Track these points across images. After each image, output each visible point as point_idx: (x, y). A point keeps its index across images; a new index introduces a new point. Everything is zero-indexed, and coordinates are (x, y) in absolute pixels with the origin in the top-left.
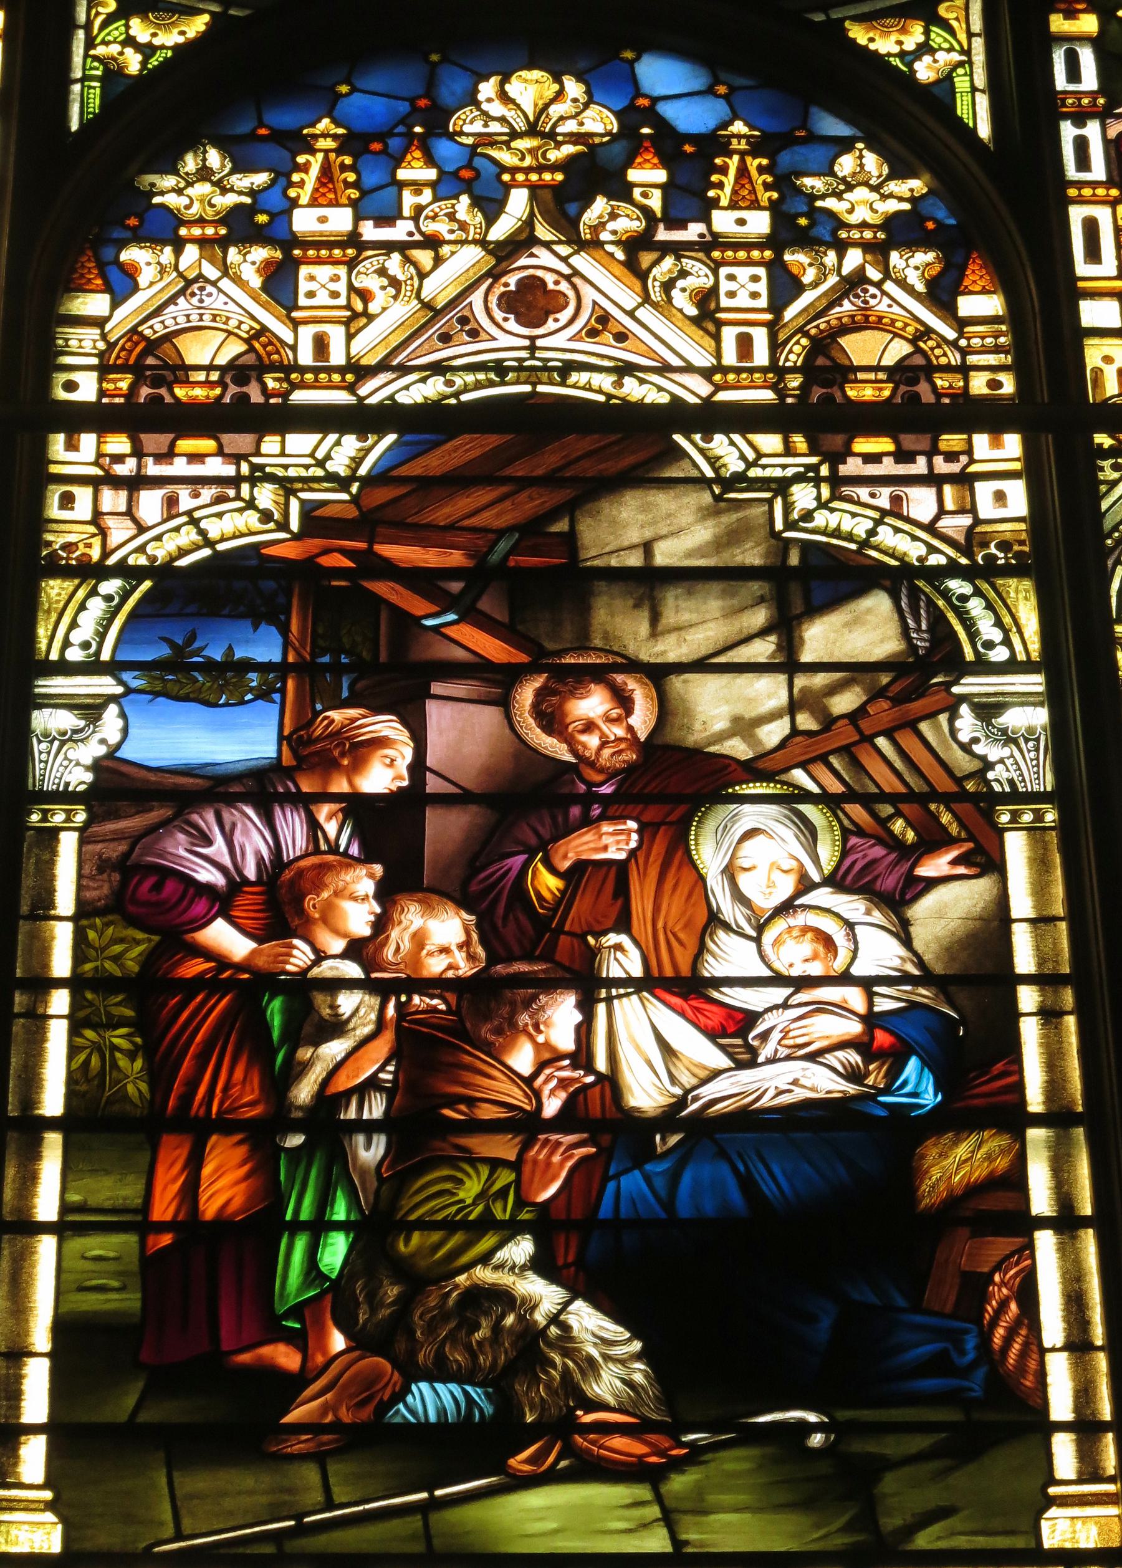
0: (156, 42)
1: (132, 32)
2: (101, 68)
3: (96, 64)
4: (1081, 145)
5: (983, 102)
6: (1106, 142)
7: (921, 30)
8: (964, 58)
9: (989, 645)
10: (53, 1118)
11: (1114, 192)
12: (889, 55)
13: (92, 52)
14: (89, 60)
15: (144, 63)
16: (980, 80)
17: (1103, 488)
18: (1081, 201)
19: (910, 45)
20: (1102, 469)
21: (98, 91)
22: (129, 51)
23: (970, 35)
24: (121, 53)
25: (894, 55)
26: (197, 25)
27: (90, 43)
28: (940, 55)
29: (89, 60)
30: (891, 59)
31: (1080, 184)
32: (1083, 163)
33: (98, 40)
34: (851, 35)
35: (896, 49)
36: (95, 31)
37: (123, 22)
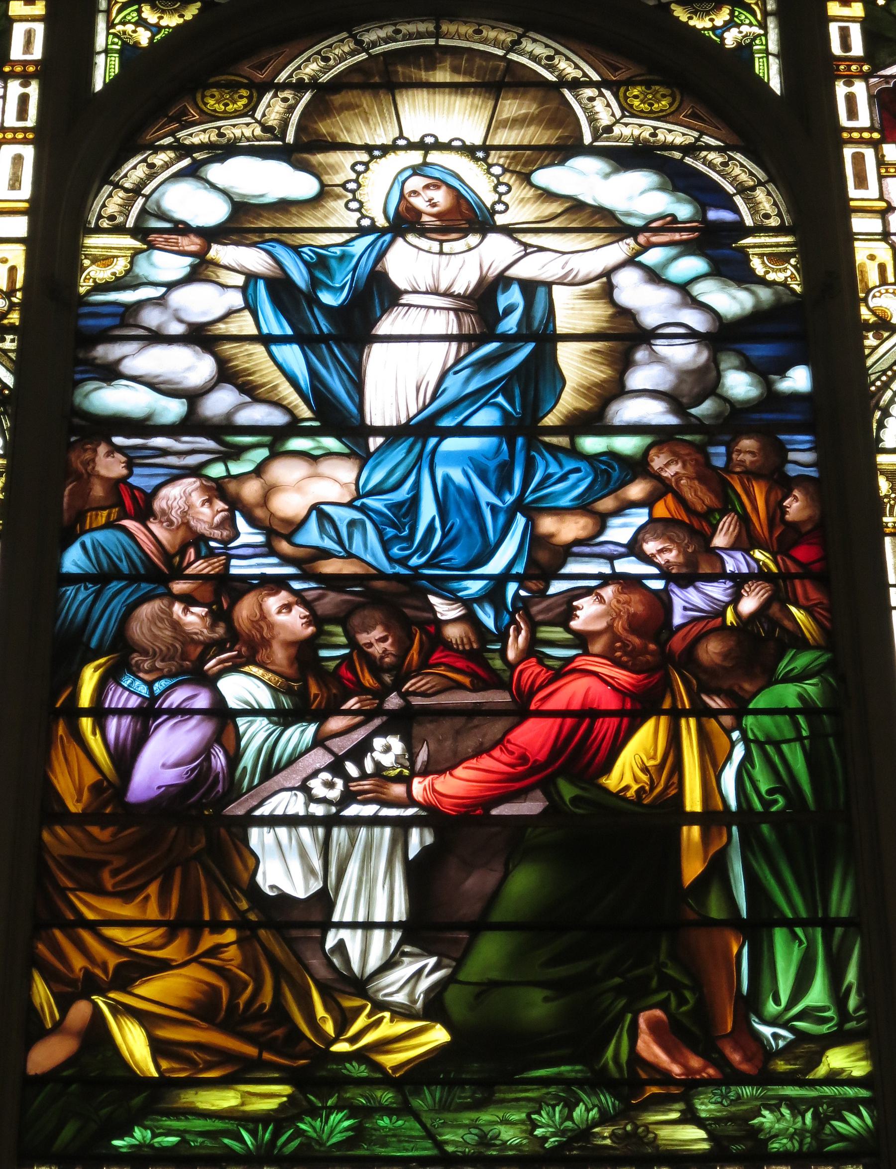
0: (163, 23)
1: (144, 15)
2: (120, 43)
3: (116, 40)
4: (851, 99)
5: (774, 65)
6: (871, 97)
7: (726, 42)
8: (762, 32)
9: (767, 216)
10: (414, 143)
11: (876, 135)
12: (705, 29)
13: (111, 31)
14: (111, 37)
15: (151, 39)
16: (773, 47)
17: (867, 352)
18: (851, 141)
19: (719, 22)
20: (866, 337)
21: (117, 59)
22: (141, 30)
23: (765, 14)
24: (135, 31)
25: (708, 29)
26: (191, 13)
27: (110, 25)
28: (743, 28)
29: (111, 37)
30: (706, 32)
31: (851, 130)
32: (852, 113)
33: (117, 21)
34: (676, 14)
35: (709, 25)
36: (114, 15)
37: (136, 7)
